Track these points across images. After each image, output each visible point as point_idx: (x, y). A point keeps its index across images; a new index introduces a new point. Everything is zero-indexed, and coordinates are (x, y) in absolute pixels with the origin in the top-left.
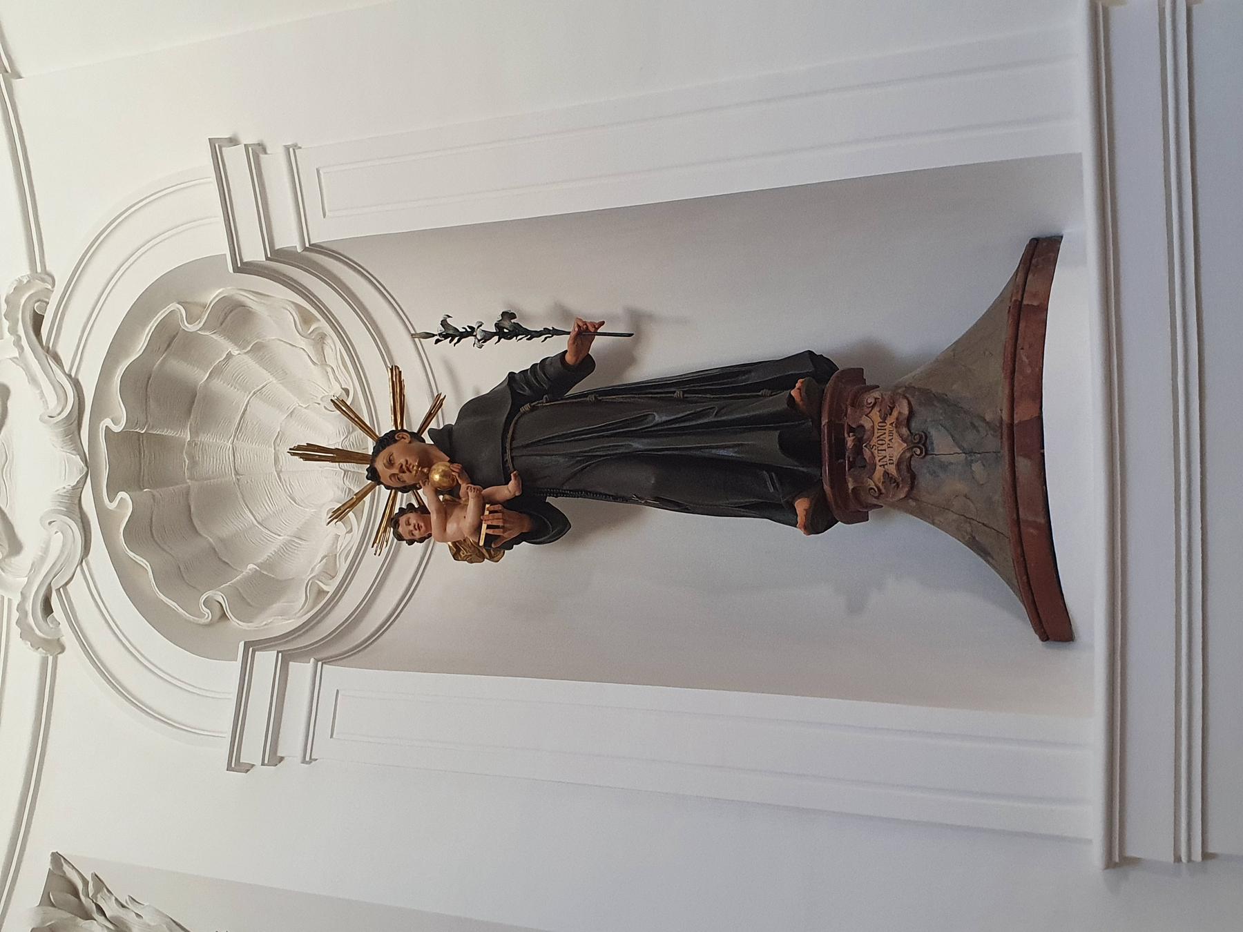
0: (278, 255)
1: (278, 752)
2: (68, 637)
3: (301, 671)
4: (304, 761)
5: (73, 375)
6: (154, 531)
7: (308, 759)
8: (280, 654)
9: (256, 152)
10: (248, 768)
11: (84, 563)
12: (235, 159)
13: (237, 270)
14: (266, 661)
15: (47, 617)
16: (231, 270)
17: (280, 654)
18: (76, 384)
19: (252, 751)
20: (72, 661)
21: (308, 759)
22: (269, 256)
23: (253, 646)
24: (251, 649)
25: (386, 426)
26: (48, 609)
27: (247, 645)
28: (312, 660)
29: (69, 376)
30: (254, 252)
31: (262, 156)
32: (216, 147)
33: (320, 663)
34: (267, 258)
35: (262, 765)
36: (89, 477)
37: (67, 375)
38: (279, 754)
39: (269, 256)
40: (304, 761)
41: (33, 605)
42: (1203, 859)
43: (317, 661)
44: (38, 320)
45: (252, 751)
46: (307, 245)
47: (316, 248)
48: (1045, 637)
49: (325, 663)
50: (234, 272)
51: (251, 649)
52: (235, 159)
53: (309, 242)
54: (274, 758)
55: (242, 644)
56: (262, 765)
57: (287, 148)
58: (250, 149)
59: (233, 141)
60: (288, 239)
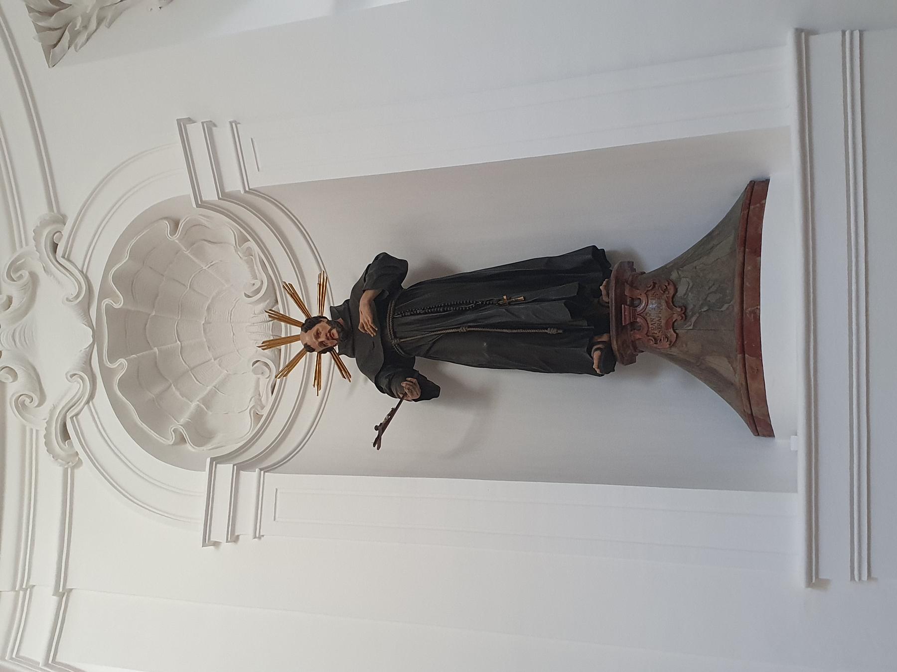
0: (225, 196)
1: (236, 531)
2: (82, 455)
3: (250, 478)
4: (255, 537)
5: (85, 271)
6: (232, 232)
7: (258, 536)
8: (235, 467)
9: (209, 127)
10: (216, 544)
11: (91, 403)
12: (196, 132)
13: (198, 206)
14: (225, 471)
15: (66, 441)
16: (194, 206)
17: (235, 467)
18: (86, 277)
19: (219, 531)
20: (85, 473)
21: (258, 536)
22: (220, 197)
23: (216, 461)
24: (214, 462)
25: (302, 319)
26: (65, 435)
27: (212, 460)
28: (257, 470)
29: (81, 272)
30: (210, 194)
31: (214, 129)
32: (183, 125)
33: (262, 472)
34: (219, 198)
35: (226, 542)
36: (95, 346)
37: (81, 271)
38: (236, 534)
39: (220, 197)
40: (255, 537)
41: (55, 429)
42: (867, 579)
43: (261, 470)
44: (55, 246)
45: (219, 531)
46: (247, 189)
47: (251, 192)
48: (757, 433)
49: (266, 472)
50: (197, 207)
51: (214, 462)
52: (196, 132)
53: (249, 187)
54: (234, 538)
55: (208, 460)
56: (226, 542)
57: (231, 123)
58: (205, 125)
59: (190, 120)
60: (234, 185)
